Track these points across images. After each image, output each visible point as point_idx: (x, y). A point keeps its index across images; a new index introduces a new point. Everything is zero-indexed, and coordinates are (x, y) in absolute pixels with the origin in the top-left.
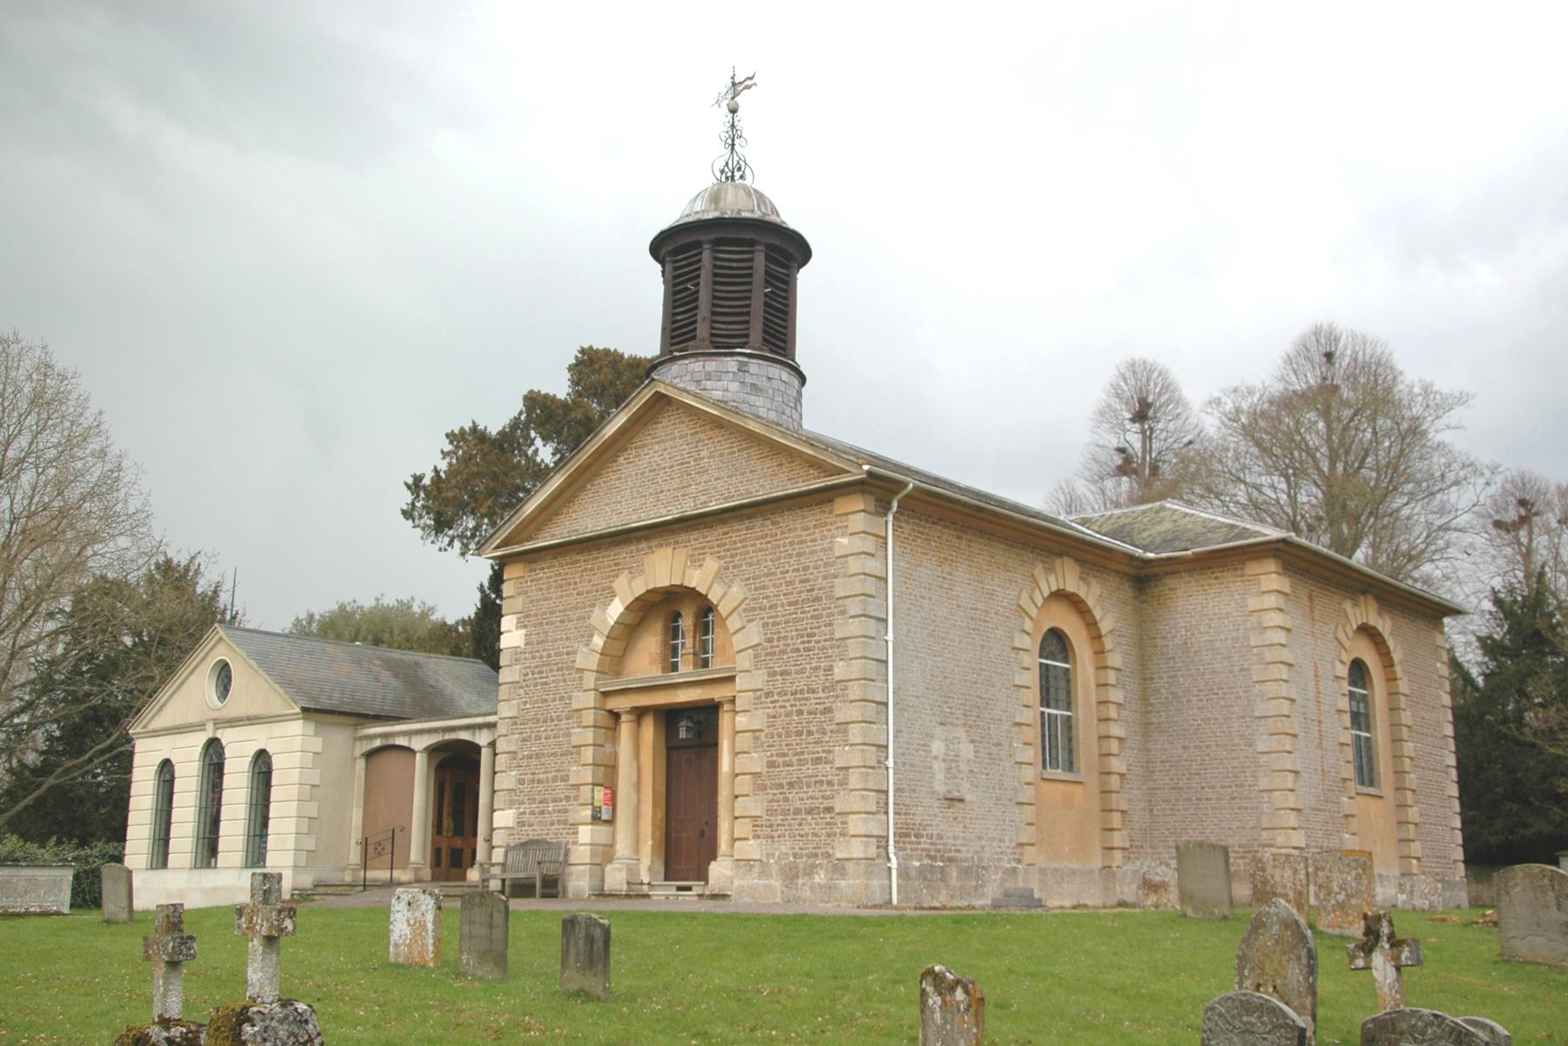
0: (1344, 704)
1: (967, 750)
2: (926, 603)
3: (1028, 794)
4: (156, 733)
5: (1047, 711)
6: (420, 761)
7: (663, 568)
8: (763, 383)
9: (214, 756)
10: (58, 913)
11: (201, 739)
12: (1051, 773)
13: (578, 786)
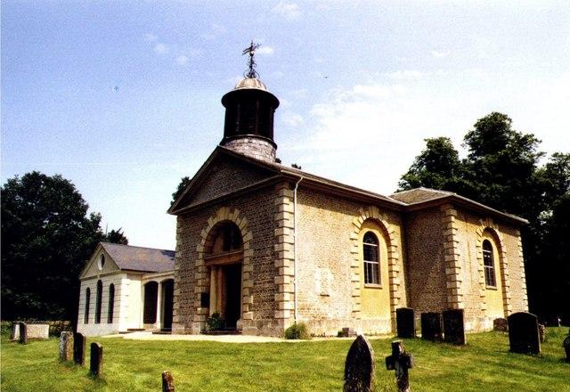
0: (481, 256)
1: (330, 277)
2: (312, 222)
3: (356, 293)
4: (86, 279)
5: (368, 262)
6: (160, 286)
7: (223, 215)
8: (258, 146)
9: (100, 285)
10: (39, 339)
11: (96, 281)
12: (369, 285)
13: (196, 294)
